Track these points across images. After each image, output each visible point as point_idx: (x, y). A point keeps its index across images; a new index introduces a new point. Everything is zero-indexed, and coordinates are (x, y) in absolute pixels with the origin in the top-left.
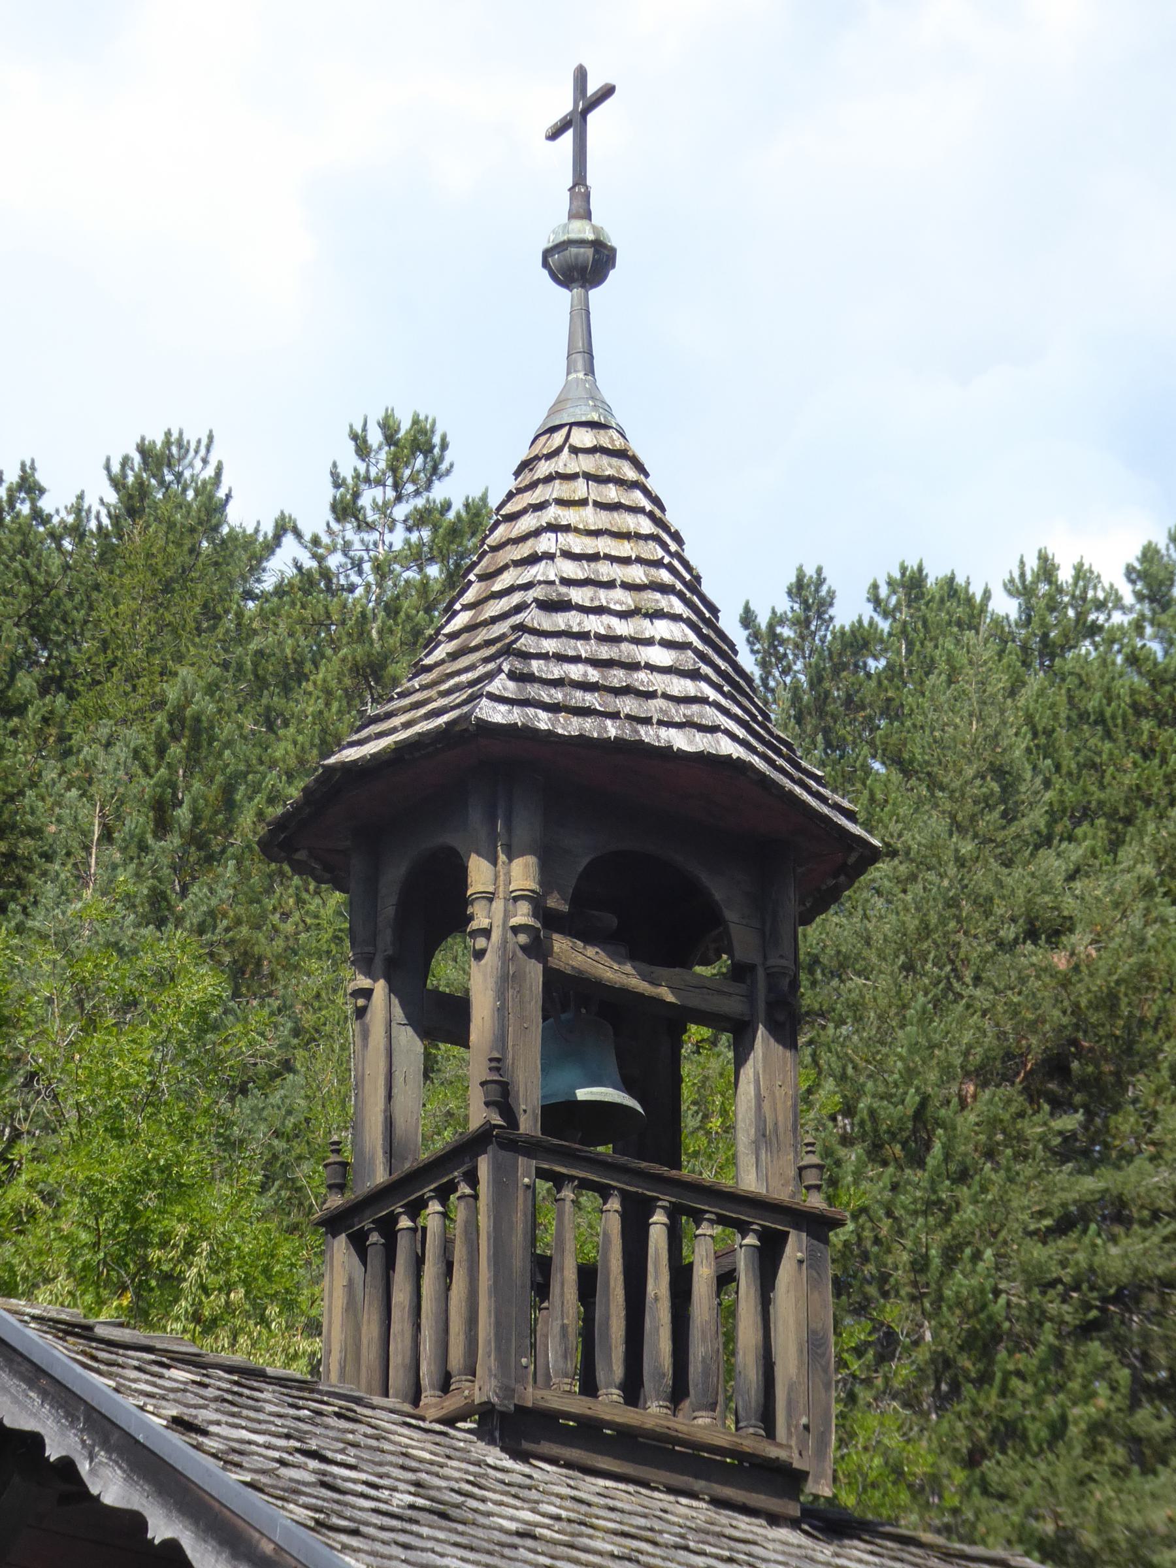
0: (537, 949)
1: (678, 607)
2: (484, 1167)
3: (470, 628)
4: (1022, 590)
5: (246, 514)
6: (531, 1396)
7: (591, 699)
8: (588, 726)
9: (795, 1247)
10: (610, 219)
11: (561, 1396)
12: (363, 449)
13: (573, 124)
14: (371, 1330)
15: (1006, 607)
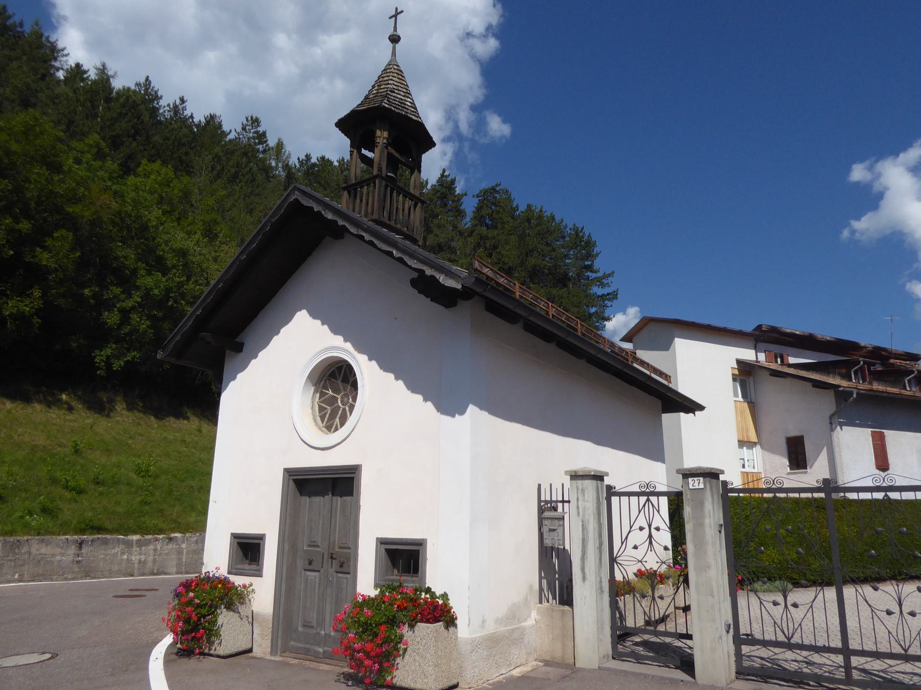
0: (386, 148)
2: (377, 181)
4: (339, 162)
5: (226, 128)
6: (382, 219)
9: (419, 205)
10: (400, 32)
11: (386, 220)
12: (247, 120)
13: (395, 16)
15: (336, 164)
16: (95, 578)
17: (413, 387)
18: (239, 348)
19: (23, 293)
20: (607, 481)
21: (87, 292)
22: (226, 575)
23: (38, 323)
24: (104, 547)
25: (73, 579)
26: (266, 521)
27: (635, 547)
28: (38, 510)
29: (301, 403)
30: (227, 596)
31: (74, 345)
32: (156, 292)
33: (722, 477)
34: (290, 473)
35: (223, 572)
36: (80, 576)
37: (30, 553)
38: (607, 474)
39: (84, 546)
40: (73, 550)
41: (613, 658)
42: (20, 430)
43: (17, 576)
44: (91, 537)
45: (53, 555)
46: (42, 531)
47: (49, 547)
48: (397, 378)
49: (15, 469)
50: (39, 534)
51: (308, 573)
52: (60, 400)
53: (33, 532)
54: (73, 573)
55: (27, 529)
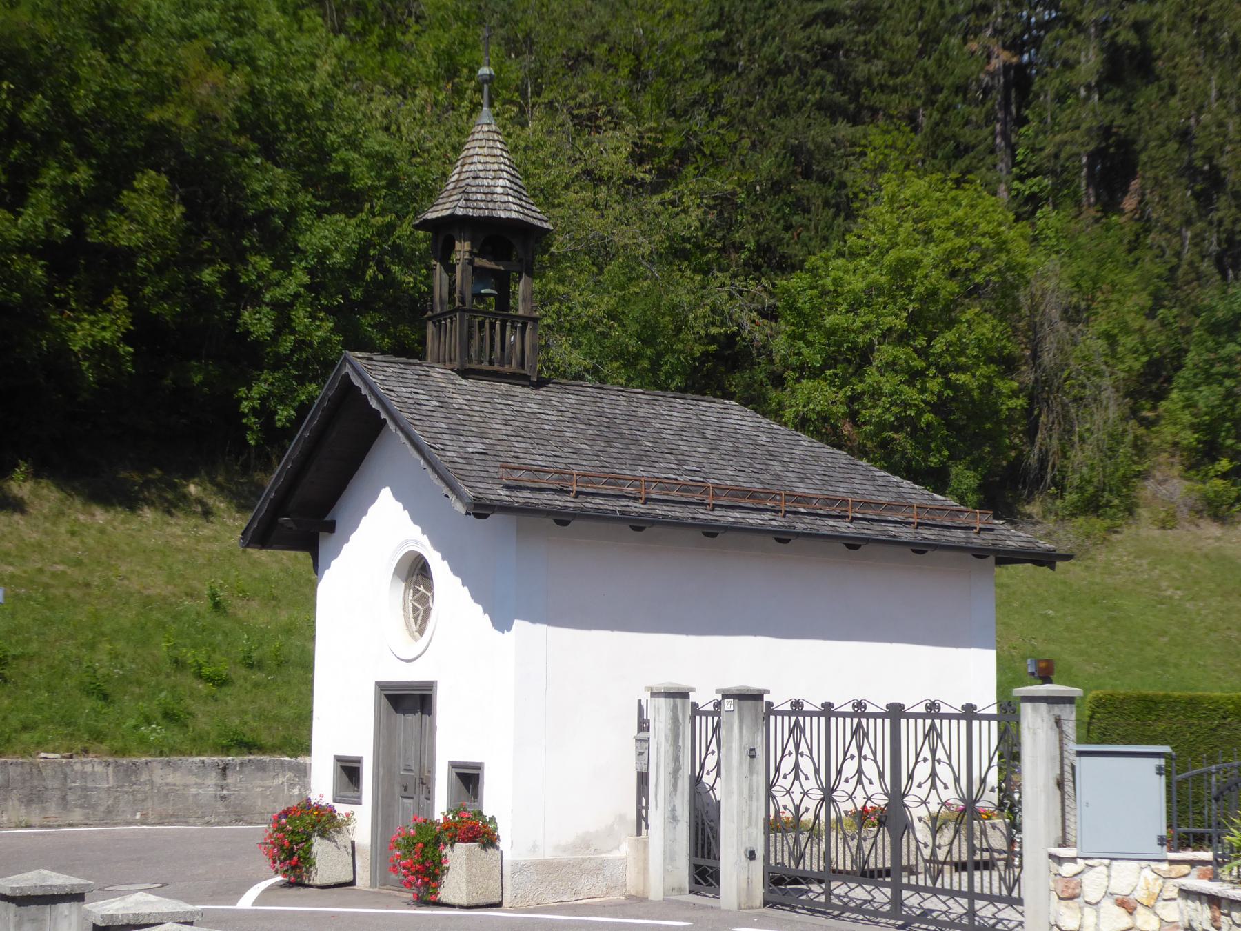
1: (505, 175)
3: (458, 181)
6: (468, 366)
7: (482, 205)
8: (481, 213)
14: (436, 345)
16: (250, 824)
17: (476, 597)
18: (331, 528)
19: (96, 302)
20: (693, 698)
21: (208, 275)
22: (331, 803)
23: (129, 354)
24: (260, 774)
25: (218, 824)
26: (363, 747)
27: (919, 786)
28: (159, 716)
29: (392, 598)
30: (324, 822)
31: (198, 378)
32: (337, 258)
33: (766, 698)
34: (381, 687)
35: (328, 800)
36: (228, 819)
37: (152, 783)
38: (693, 690)
39: (229, 772)
40: (213, 779)
41: (690, 892)
42: (124, 568)
43: (138, 816)
44: (238, 759)
45: (186, 786)
46: (166, 749)
47: (178, 774)
48: (464, 584)
49: (120, 645)
50: (161, 754)
51: (405, 800)
52: (185, 497)
53: (153, 751)
54: (217, 814)
55: (145, 746)
